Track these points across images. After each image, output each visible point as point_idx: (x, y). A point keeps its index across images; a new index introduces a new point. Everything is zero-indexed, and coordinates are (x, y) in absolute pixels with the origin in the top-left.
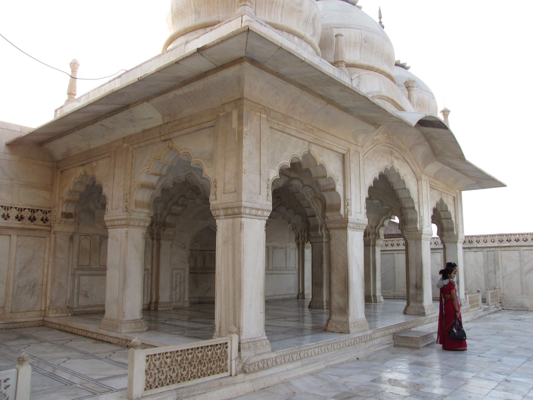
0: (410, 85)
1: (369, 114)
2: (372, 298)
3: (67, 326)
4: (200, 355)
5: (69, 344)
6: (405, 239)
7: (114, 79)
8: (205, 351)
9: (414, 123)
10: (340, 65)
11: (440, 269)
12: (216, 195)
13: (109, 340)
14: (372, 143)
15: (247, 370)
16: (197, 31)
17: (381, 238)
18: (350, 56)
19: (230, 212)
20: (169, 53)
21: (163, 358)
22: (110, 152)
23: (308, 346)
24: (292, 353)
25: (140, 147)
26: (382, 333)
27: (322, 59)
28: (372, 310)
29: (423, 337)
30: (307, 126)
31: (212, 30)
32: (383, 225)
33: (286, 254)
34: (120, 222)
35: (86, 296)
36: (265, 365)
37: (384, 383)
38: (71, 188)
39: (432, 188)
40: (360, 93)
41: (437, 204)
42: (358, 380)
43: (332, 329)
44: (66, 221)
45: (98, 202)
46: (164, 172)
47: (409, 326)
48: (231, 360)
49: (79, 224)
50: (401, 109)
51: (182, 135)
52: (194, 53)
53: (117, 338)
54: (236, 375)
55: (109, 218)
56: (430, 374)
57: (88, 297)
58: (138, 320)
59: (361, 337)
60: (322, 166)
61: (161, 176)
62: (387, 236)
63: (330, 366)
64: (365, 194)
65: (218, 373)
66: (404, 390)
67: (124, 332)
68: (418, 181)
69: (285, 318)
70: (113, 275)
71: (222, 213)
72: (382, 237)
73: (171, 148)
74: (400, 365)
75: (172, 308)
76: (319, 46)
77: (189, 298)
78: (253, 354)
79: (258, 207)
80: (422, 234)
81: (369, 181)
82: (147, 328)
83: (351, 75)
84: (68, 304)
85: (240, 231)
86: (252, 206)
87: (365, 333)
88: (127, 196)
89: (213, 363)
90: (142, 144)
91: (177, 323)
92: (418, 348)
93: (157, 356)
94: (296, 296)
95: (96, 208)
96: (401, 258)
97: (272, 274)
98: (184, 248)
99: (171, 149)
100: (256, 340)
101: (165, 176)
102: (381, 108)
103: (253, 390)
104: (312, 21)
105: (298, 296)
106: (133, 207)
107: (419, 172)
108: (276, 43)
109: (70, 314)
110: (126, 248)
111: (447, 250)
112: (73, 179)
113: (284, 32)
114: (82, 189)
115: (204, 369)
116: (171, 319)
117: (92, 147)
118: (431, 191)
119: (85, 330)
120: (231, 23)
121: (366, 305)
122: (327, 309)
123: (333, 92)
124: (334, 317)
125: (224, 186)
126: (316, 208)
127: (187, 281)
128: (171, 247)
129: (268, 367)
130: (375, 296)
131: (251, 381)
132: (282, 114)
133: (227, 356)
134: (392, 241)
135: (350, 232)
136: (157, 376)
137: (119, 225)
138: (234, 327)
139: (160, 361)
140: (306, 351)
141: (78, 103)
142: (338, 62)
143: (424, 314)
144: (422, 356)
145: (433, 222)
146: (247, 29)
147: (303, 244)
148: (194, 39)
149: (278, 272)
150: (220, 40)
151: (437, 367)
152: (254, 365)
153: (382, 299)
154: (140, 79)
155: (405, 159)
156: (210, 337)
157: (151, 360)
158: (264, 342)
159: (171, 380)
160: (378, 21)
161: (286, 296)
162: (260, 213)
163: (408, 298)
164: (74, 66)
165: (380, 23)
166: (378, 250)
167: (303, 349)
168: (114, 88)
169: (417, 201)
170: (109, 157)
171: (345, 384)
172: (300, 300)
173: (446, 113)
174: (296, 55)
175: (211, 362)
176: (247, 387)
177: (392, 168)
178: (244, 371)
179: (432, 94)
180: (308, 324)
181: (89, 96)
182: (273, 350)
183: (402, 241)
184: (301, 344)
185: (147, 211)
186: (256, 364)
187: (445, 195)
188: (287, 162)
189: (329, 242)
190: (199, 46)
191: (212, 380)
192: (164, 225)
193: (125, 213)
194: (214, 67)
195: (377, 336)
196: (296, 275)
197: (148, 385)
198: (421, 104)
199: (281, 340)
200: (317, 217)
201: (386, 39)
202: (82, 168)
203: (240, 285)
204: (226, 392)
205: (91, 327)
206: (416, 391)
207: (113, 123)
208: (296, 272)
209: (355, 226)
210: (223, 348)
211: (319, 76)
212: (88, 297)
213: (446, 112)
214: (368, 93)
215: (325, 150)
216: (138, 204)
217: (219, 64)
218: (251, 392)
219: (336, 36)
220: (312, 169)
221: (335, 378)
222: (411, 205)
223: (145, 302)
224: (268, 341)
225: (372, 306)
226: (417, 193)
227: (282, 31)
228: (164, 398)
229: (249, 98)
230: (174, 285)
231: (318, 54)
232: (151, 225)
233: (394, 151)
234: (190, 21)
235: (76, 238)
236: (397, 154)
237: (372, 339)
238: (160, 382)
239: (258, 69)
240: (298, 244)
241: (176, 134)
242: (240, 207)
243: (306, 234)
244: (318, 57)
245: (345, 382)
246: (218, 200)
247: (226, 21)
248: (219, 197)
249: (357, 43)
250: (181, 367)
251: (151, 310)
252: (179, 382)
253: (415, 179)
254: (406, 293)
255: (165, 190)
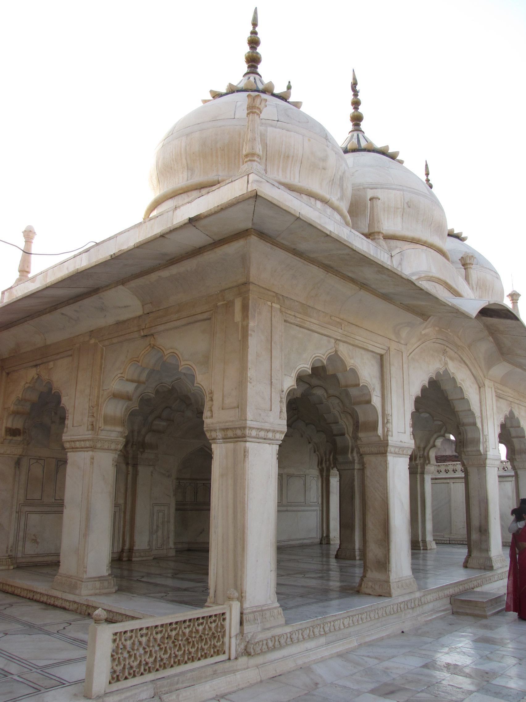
0: (468, 262)
1: (414, 302)
2: (421, 544)
3: (6, 584)
4: (187, 631)
5: (8, 611)
6: (463, 465)
7: (80, 254)
8: (194, 625)
9: (474, 313)
10: (377, 237)
11: (512, 508)
12: (211, 411)
13: (64, 605)
14: (420, 340)
15: (252, 651)
16: (189, 194)
17: (431, 462)
18: (389, 225)
19: (230, 433)
20: (153, 220)
21: (136, 637)
22: (73, 349)
23: (335, 616)
24: (312, 627)
25: (113, 344)
26: (435, 595)
27: (353, 230)
28: (421, 562)
29: (491, 600)
30: (333, 318)
31: (208, 193)
32: (434, 446)
33: (305, 484)
34: (83, 444)
35: (35, 541)
36: (276, 644)
37: (440, 670)
38: (20, 396)
39: (498, 397)
40: (404, 276)
41: (506, 418)
42: (405, 664)
43: (368, 591)
44: (12, 440)
45: (56, 413)
46: (143, 378)
47: (471, 585)
48: (230, 637)
49: (28, 444)
50: (457, 294)
51: (167, 330)
52: (185, 224)
53: (75, 602)
54: (236, 658)
55: (69, 438)
56: (503, 657)
57: (38, 543)
58: (104, 576)
59: (407, 601)
60: (353, 371)
61: (139, 382)
62: (440, 459)
63: (366, 643)
64: (410, 407)
65: (212, 656)
66: (468, 680)
67: (85, 594)
68: (480, 388)
69: (303, 573)
70: (72, 515)
71: (220, 435)
72: (433, 461)
73: (153, 347)
74: (460, 642)
75: (151, 558)
76: (349, 212)
77: (175, 543)
78: (259, 629)
79: (268, 428)
80: (486, 459)
81: (415, 390)
82: (117, 588)
83: (390, 249)
84: (10, 553)
85: (244, 460)
86: (260, 427)
87: (413, 596)
88: (95, 408)
89: (203, 642)
90: (115, 340)
91: (158, 580)
92: (485, 617)
93: (129, 634)
94: (318, 540)
95: (53, 422)
96: (458, 489)
97: (287, 511)
98: (169, 476)
99: (153, 348)
100: (264, 608)
101: (144, 383)
102: (430, 295)
103: (259, 680)
104: (339, 181)
105: (321, 540)
106: (101, 424)
107: (482, 376)
108: (293, 212)
109: (12, 567)
110: (90, 482)
111: (520, 480)
112: (23, 383)
113: (303, 195)
114: (34, 397)
115: (193, 650)
116: (149, 575)
117: (49, 342)
118: (497, 400)
119: (31, 591)
120: (234, 183)
121: (413, 554)
122: (360, 560)
123: (368, 274)
124: (369, 574)
125: (223, 399)
126: (346, 424)
127: (172, 521)
128: (152, 475)
129: (281, 647)
130: (424, 541)
131: (257, 666)
132: (300, 303)
133: (225, 632)
134: (447, 465)
135: (391, 459)
136: (127, 663)
137: (82, 448)
138: (235, 591)
139: (132, 641)
140: (332, 623)
141: (33, 284)
142: (373, 233)
143: (491, 568)
144: (491, 629)
145: (500, 442)
146: (254, 193)
147: (328, 471)
148: (186, 204)
149: (294, 508)
150: (219, 208)
151: (510, 646)
152: (261, 643)
153: (434, 545)
154: (113, 256)
155: (462, 359)
156: (201, 603)
157: (120, 640)
158: (276, 611)
159: (147, 668)
160: (424, 178)
161: (305, 541)
162: (270, 435)
163: (468, 544)
164: (29, 235)
165: (428, 180)
166: (428, 478)
167: (329, 620)
168: (78, 267)
169: (479, 415)
170: (71, 355)
171: (386, 671)
172: (324, 546)
173: (515, 298)
174: (319, 227)
175: (202, 640)
176: (252, 675)
177: (446, 371)
178: (247, 653)
179: (496, 273)
180: (335, 584)
181: (47, 274)
182: (287, 623)
183: (458, 466)
184: (326, 613)
185: (119, 429)
186: (265, 642)
187: (516, 405)
188: (306, 366)
189: (362, 470)
190: (192, 216)
191: (202, 667)
192: (143, 446)
193: (90, 432)
194: (211, 241)
195: (429, 600)
196: (319, 513)
197: (115, 676)
198: (482, 287)
199: (297, 606)
200: (346, 435)
201: (435, 202)
202: (35, 369)
203: (243, 533)
204: (220, 684)
205: (40, 586)
206: (485, 683)
207: (76, 311)
208: (318, 508)
209: (397, 450)
210: (219, 620)
211: (349, 255)
212: (38, 543)
213: (514, 296)
214: (413, 274)
215: (357, 349)
216: (108, 420)
217: (217, 238)
218: (257, 683)
219: (370, 200)
220: (340, 376)
221: (372, 662)
222: (471, 420)
223: (116, 550)
224: (280, 610)
225: (421, 555)
226: (478, 405)
227: (301, 193)
228: (136, 694)
229: (256, 282)
230: (155, 527)
231: (347, 224)
232: (126, 446)
233: (448, 349)
234: (180, 180)
235: (24, 462)
236: (451, 353)
237: (421, 604)
238: (132, 671)
239: (268, 244)
240: (321, 471)
241: (162, 328)
242: (244, 428)
243: (331, 457)
244: (347, 227)
245: (387, 668)
246: (214, 418)
247: (227, 181)
248: (215, 415)
249: (398, 208)
250: (161, 649)
251: (123, 560)
252: (157, 670)
253: (476, 386)
254: (466, 536)
255: (144, 401)
